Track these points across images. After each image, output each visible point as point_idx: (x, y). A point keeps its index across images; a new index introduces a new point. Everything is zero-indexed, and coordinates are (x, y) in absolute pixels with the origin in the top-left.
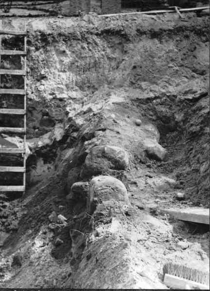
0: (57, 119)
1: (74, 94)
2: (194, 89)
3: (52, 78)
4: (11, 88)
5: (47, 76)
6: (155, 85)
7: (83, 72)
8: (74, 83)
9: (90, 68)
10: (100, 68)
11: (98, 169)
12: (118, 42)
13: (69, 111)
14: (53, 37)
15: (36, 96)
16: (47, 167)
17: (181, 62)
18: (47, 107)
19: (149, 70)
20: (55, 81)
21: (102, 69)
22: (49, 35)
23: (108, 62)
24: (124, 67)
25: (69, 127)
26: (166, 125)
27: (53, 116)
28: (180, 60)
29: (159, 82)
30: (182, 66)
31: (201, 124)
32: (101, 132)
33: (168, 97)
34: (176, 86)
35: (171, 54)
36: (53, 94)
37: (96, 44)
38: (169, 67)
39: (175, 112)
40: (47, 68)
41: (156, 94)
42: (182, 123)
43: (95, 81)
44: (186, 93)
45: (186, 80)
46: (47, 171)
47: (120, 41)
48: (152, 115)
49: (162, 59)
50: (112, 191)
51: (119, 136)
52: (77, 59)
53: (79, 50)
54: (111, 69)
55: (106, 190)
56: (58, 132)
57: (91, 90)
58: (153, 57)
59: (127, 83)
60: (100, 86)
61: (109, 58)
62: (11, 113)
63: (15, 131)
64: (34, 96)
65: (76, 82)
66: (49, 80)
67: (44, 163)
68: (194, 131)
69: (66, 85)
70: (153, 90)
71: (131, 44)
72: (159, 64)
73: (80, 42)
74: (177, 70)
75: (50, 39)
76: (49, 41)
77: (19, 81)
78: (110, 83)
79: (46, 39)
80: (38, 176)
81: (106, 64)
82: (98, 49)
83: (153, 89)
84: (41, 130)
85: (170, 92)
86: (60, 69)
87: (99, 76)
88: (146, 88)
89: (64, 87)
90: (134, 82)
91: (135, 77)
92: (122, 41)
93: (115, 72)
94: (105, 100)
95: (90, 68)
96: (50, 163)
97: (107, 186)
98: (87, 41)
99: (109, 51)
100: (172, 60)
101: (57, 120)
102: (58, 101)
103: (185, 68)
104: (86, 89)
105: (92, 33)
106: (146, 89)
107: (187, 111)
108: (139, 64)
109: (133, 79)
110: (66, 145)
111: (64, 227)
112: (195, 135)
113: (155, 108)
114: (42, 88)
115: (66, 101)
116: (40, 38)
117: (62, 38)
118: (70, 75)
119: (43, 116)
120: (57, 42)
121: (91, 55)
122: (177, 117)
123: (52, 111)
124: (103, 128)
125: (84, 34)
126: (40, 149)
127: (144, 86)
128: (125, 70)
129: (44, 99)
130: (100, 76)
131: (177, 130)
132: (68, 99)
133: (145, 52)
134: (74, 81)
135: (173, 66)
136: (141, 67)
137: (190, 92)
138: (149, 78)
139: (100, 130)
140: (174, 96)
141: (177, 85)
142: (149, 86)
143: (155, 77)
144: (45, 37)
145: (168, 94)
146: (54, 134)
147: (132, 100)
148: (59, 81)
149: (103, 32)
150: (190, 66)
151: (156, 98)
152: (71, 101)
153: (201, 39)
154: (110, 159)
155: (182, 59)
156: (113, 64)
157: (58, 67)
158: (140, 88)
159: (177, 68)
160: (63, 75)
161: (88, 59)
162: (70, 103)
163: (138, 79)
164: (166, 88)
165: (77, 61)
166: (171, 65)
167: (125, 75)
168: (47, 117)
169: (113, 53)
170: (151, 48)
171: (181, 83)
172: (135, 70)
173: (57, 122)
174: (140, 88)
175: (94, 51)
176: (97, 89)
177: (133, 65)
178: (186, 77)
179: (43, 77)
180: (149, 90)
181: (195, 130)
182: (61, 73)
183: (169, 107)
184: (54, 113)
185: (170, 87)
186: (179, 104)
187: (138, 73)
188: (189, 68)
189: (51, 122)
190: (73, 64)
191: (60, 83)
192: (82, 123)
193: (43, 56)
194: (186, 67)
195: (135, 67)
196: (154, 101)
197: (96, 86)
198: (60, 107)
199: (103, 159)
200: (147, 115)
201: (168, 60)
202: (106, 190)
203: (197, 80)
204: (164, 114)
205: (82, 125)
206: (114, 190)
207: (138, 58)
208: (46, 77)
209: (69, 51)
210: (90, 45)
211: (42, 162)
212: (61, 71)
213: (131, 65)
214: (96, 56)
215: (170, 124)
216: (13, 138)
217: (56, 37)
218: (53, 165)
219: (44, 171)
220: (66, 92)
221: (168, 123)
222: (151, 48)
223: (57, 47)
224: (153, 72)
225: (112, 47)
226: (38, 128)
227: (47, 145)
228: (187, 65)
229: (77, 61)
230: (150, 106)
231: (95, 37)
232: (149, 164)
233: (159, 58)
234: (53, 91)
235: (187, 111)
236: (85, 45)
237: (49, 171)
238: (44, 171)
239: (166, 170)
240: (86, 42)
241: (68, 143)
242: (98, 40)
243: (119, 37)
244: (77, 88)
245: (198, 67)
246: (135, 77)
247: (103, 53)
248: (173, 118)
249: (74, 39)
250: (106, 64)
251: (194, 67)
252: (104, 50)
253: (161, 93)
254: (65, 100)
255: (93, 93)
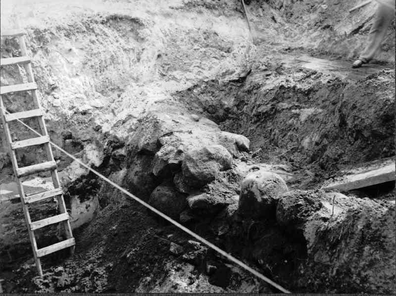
0: (84, 139)
1: (99, 102)
2: (231, 69)
3: (65, 88)
4: (17, 111)
5: (58, 85)
6: (188, 73)
7: (100, 72)
8: (94, 89)
9: (107, 66)
10: (119, 64)
11: (211, 175)
12: (130, 29)
13: (101, 125)
14: (51, 33)
15: (54, 114)
16: (85, 206)
17: (205, 42)
18: (69, 126)
19: (176, 57)
20: (69, 91)
21: (122, 65)
22: (45, 31)
23: (125, 55)
24: (148, 57)
25: (107, 145)
26: (214, 115)
27: (79, 137)
28: (204, 40)
29: (191, 68)
30: (207, 46)
31: (273, 101)
32: (167, 137)
33: (207, 83)
34: (209, 70)
35: (192, 35)
36: (73, 107)
37: (106, 35)
38: (195, 50)
39: (221, 98)
40: (55, 75)
41: (194, 82)
42: (235, 109)
43: (118, 82)
44: (224, 75)
45: (216, 61)
46: (86, 212)
47: (132, 27)
48: (197, 108)
49: (185, 42)
50: (275, 183)
51: (320, 105)
52: (89, 58)
53: (89, 45)
54: (132, 64)
55: (270, 185)
56: (94, 156)
57: (117, 93)
58: (174, 41)
59: (157, 75)
60: (125, 86)
61: (125, 50)
62: (22, 146)
63: (43, 168)
64: (51, 115)
65: (96, 86)
66: (62, 91)
67: (81, 202)
68: (264, 111)
69: (85, 93)
70: (189, 79)
71: (146, 29)
72: (184, 48)
73: (86, 35)
74: (205, 52)
75: (48, 36)
76: (47, 39)
77: (27, 99)
78: (137, 80)
79: (42, 37)
80: (75, 222)
81: (123, 57)
82: (110, 41)
83: (188, 78)
84: (64, 160)
85: (207, 78)
86: (71, 74)
87: (121, 75)
88: (181, 77)
89: (83, 96)
90: (164, 74)
91: (163, 67)
92: (134, 27)
93: (137, 66)
94: (143, 101)
95: (107, 66)
96: (88, 199)
97: (268, 180)
98: (94, 32)
99: (122, 41)
100: (196, 41)
101: (84, 141)
102: (81, 116)
103: (210, 48)
104: (110, 93)
105: (96, 22)
106: (181, 79)
107: (237, 94)
108: (163, 51)
109: (161, 71)
110: (109, 169)
111: (206, 252)
112: (266, 115)
113: (198, 99)
114: (57, 103)
115: (91, 113)
116: (34, 36)
117: (63, 33)
118: (85, 80)
119: (65, 139)
120: (57, 38)
121: (104, 49)
122: (226, 103)
123: (75, 130)
124: (167, 131)
125: (89, 24)
126: (74, 184)
127: (178, 77)
128: (150, 61)
129: (64, 116)
130: (122, 74)
131: (229, 118)
132: (94, 110)
133: (166, 36)
134: (93, 86)
135: (198, 48)
136: (166, 55)
137: (227, 73)
138: (180, 66)
139: (164, 136)
140: (213, 81)
141: (210, 69)
142: (182, 75)
143: (185, 63)
144: (41, 34)
145: (206, 80)
146: (89, 160)
147: (172, 95)
148: (74, 90)
149: (108, 20)
150: (214, 45)
151: (195, 86)
152: (97, 111)
153: (214, 14)
154: (218, 160)
155: (205, 39)
156: (133, 56)
157: (67, 71)
158: (174, 78)
159: (203, 49)
160: (77, 81)
161: (102, 54)
162: (98, 114)
163: (168, 70)
164: (201, 74)
165: (90, 60)
166: (196, 47)
167: (151, 67)
168: (71, 140)
169: (128, 42)
170: (170, 31)
171: (213, 65)
172: (160, 59)
173: (85, 143)
174: (174, 78)
175: (106, 44)
176: (123, 91)
177: (157, 54)
178: (215, 58)
179: (54, 88)
180: (185, 80)
181: (266, 110)
182: (73, 79)
183: (210, 94)
184: (81, 133)
185: (204, 72)
186: (224, 88)
187: (166, 63)
188: (214, 47)
189: (77, 146)
190: (86, 64)
191: (76, 91)
192: (126, 136)
193: (45, 60)
194: (212, 46)
195: (159, 56)
196: (195, 91)
197: (121, 87)
198: (85, 123)
199: (211, 162)
200: (192, 108)
201: (192, 42)
202: (270, 185)
203: (228, 59)
204: (211, 104)
205: (128, 137)
206: (276, 182)
207: (159, 45)
208: (56, 88)
209: (77, 48)
210: (99, 37)
211: (78, 201)
212: (74, 76)
213: (154, 53)
214: (111, 49)
215: (217, 114)
216: (33, 181)
217: (54, 32)
218: (92, 201)
219: (81, 213)
220: (87, 102)
221: (214, 113)
222: (170, 31)
223: (59, 45)
224: (181, 58)
225: (124, 36)
226: (60, 158)
227: (83, 177)
228: (212, 45)
229: (90, 60)
230: (191, 97)
231: (101, 26)
232: (242, 157)
233: (182, 40)
234: (72, 104)
235: (237, 94)
236: (94, 38)
237: (88, 211)
238: (81, 213)
239: (263, 158)
240: (93, 34)
241: (111, 165)
242: (106, 30)
243: (128, 22)
244: (99, 94)
245: (223, 45)
246: (163, 67)
247: (118, 44)
248: (221, 105)
249: (78, 32)
250: (123, 57)
251: (219, 46)
252: (117, 41)
253: (199, 80)
254: (90, 111)
255: (119, 96)
